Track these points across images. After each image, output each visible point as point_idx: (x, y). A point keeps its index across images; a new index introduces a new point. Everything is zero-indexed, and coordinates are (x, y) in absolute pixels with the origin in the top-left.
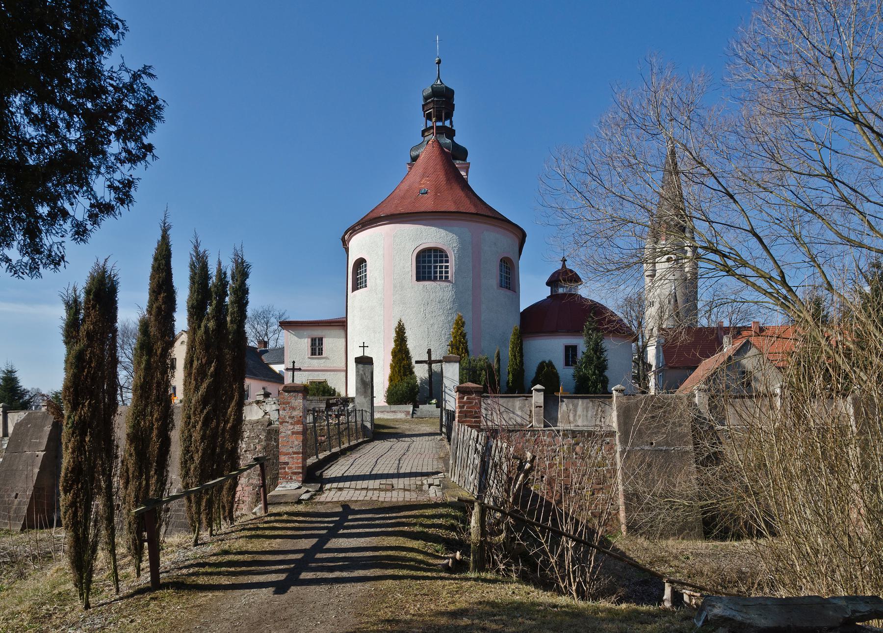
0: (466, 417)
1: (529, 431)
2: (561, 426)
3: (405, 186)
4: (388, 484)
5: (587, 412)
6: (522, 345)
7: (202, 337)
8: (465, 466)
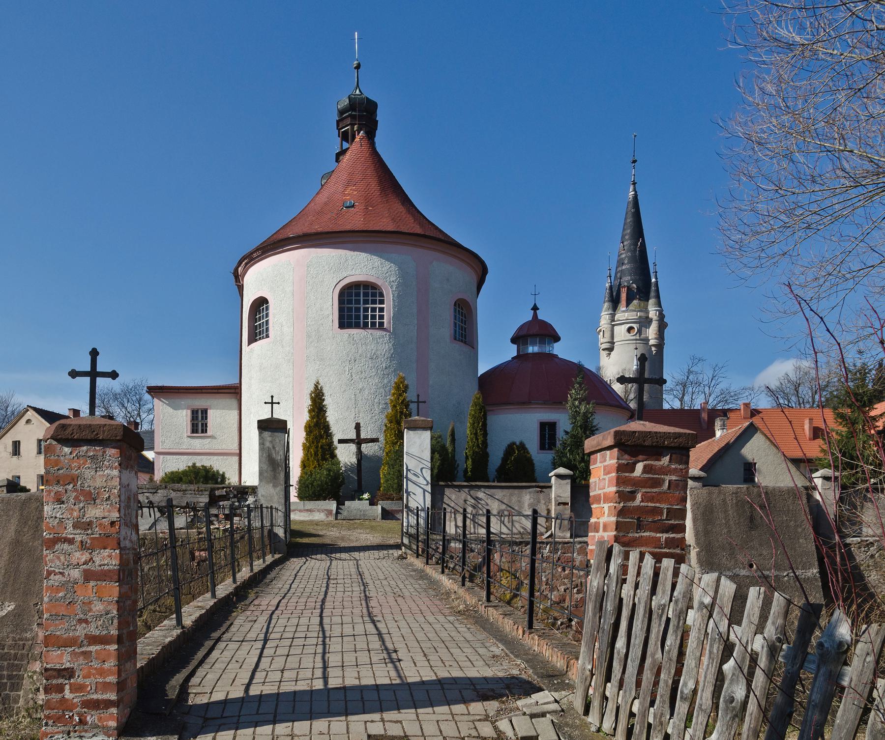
0: (640, 527)
1: (547, 543)
3: (323, 198)
6: (485, 419)
8: (663, 690)
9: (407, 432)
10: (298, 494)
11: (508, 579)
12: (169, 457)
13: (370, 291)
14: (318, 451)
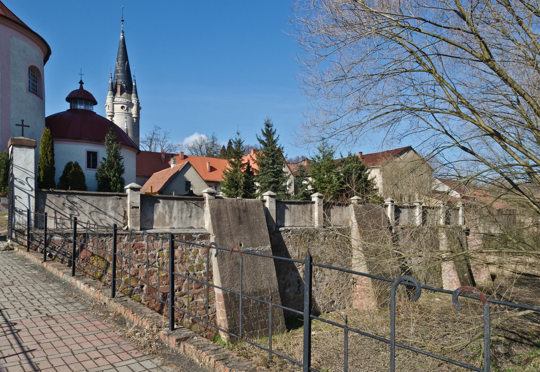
2: (157, 229)
5: (182, 213)
6: (53, 146)
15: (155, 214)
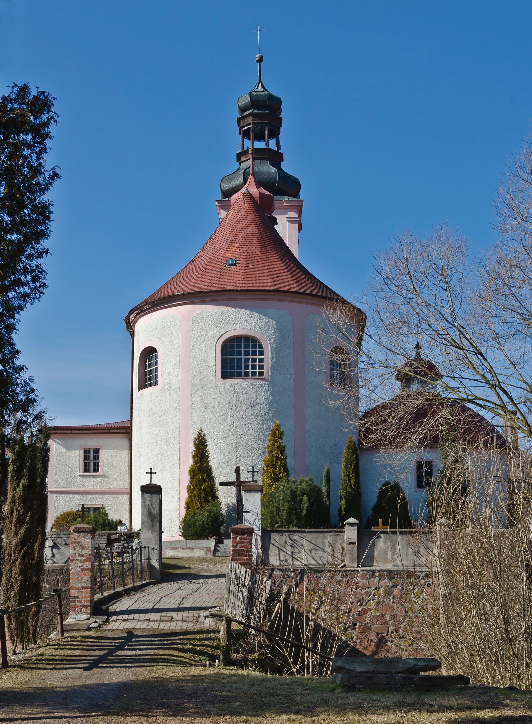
0: (239, 555)
1: (340, 571)
2: (378, 565)
3: (208, 254)
4: (168, 616)
7: (21, 494)
8: (236, 599)
9: (244, 493)
10: (182, 533)
11: (313, 596)
12: (61, 496)
13: (250, 343)
14: (201, 493)
15: (375, 550)
